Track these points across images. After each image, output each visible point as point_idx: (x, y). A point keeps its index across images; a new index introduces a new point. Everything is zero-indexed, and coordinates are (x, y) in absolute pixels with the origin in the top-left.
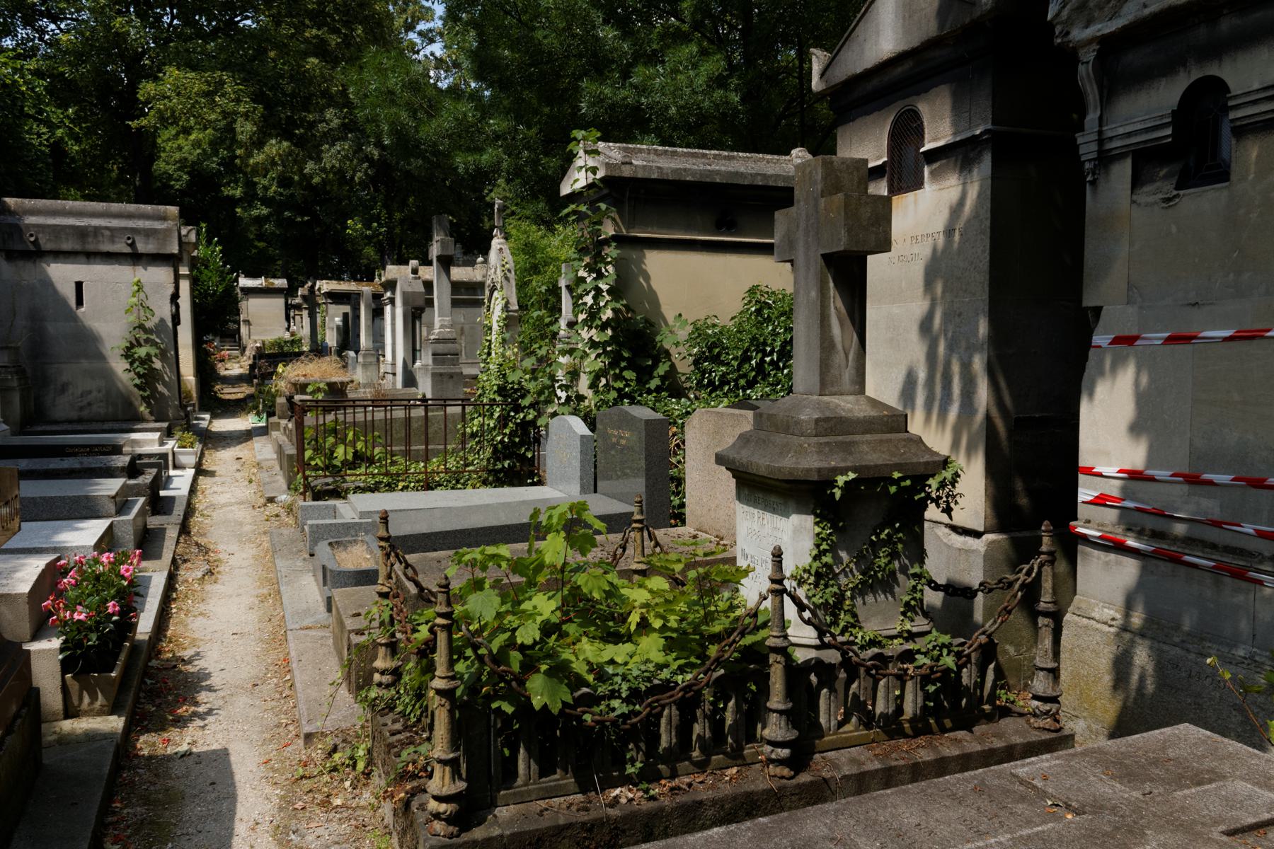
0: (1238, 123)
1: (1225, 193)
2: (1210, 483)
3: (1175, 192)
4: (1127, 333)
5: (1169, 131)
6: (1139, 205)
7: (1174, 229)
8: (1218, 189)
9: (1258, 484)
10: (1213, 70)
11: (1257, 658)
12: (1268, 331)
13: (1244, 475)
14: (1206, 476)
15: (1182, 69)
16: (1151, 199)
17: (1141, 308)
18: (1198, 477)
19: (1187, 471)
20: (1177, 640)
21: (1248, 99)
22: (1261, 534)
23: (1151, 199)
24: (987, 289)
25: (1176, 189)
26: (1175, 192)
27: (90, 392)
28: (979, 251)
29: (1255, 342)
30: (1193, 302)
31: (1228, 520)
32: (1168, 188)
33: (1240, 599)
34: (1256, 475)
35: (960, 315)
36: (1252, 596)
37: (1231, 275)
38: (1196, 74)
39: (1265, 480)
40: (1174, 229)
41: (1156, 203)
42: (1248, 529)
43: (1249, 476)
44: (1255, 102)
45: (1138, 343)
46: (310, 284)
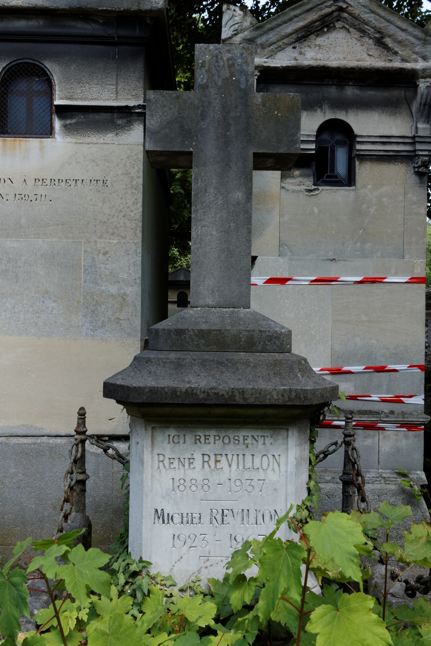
0: (362, 153)
1: (353, 193)
2: (350, 372)
3: (313, 187)
4: (279, 276)
5: (313, 146)
6: (287, 190)
7: (316, 210)
8: (348, 190)
9: (381, 370)
10: (341, 116)
11: (384, 475)
12: (385, 278)
13: (370, 365)
14: (345, 368)
15: (319, 110)
16: (297, 188)
17: (291, 259)
18: (340, 370)
19: (329, 367)
20: (328, 478)
21: (370, 140)
22: (384, 401)
23: (297, 188)
24: (140, 235)
25: (314, 185)
26: (313, 187)
27: (421, 628)
28: (130, 203)
29: (375, 285)
30: (332, 258)
31: (360, 394)
32: (309, 183)
33: (369, 442)
34: (378, 365)
35: (105, 254)
36: (376, 439)
37: (358, 244)
38: (329, 115)
39: (386, 367)
40: (316, 210)
41: (301, 191)
42: (375, 397)
43: (373, 365)
44: (373, 143)
45: (289, 283)
46: (178, 19)
